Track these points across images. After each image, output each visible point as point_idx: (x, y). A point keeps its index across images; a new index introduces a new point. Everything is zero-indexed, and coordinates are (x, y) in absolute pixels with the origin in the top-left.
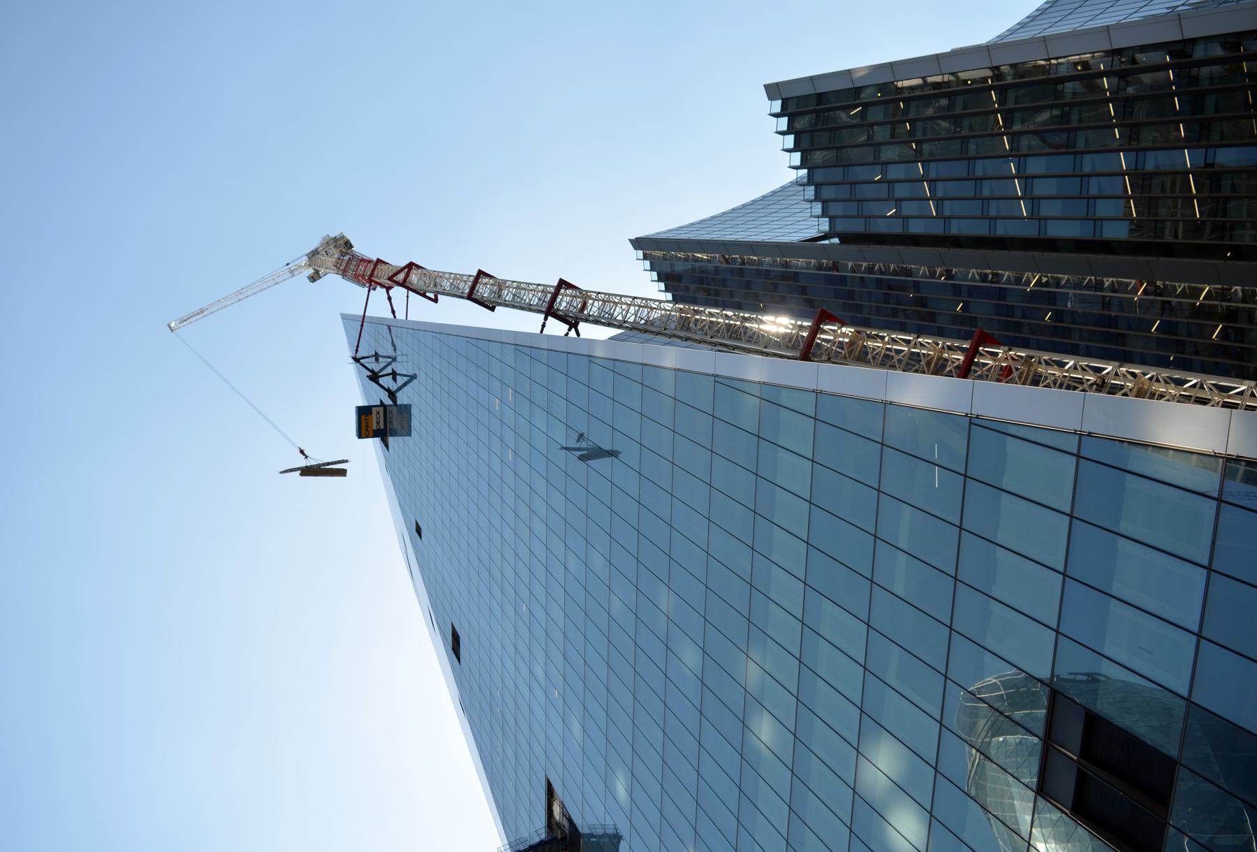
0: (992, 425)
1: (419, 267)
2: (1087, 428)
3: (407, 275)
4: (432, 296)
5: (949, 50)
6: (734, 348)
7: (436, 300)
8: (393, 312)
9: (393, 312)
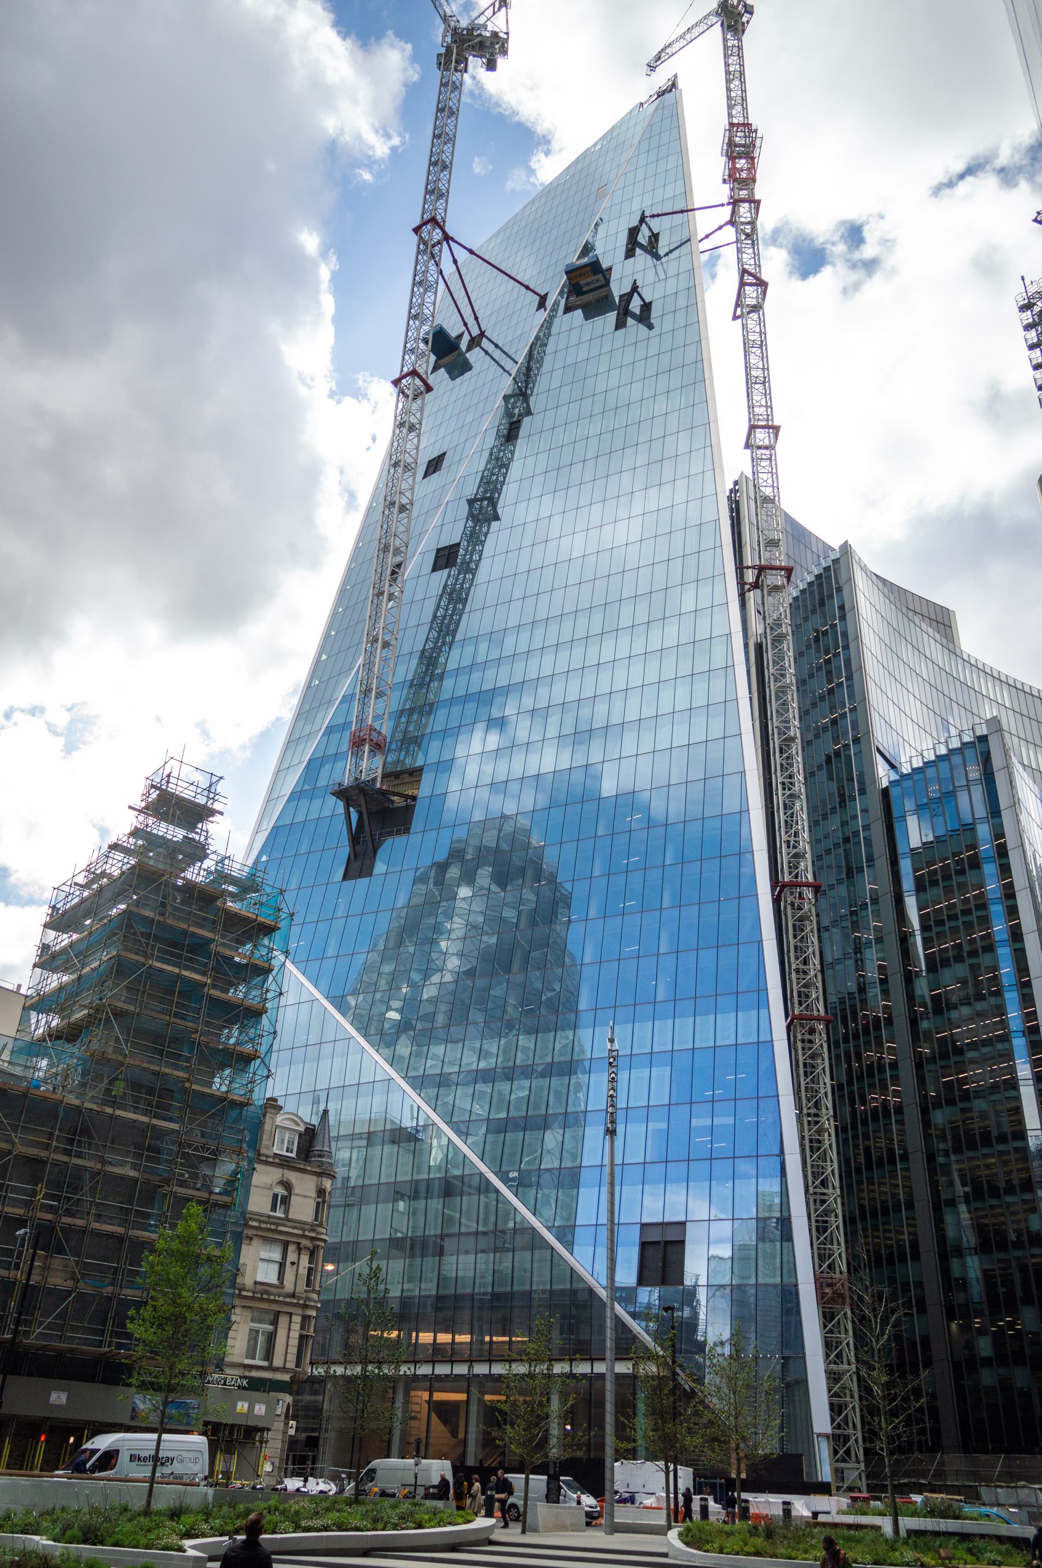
0: (761, 971)
1: (764, 292)
2: (775, 1043)
3: (751, 285)
4: (739, 313)
5: (812, 1496)
6: (812, 1249)
7: (735, 318)
8: (707, 236)
9: (707, 236)
